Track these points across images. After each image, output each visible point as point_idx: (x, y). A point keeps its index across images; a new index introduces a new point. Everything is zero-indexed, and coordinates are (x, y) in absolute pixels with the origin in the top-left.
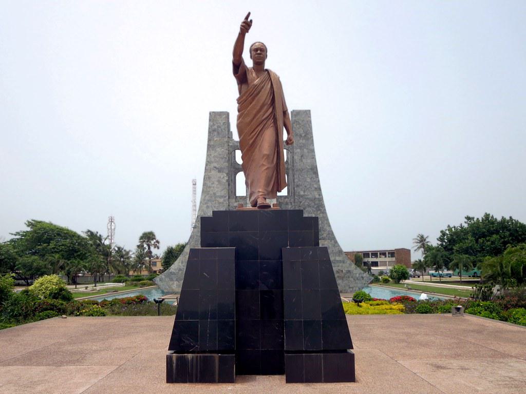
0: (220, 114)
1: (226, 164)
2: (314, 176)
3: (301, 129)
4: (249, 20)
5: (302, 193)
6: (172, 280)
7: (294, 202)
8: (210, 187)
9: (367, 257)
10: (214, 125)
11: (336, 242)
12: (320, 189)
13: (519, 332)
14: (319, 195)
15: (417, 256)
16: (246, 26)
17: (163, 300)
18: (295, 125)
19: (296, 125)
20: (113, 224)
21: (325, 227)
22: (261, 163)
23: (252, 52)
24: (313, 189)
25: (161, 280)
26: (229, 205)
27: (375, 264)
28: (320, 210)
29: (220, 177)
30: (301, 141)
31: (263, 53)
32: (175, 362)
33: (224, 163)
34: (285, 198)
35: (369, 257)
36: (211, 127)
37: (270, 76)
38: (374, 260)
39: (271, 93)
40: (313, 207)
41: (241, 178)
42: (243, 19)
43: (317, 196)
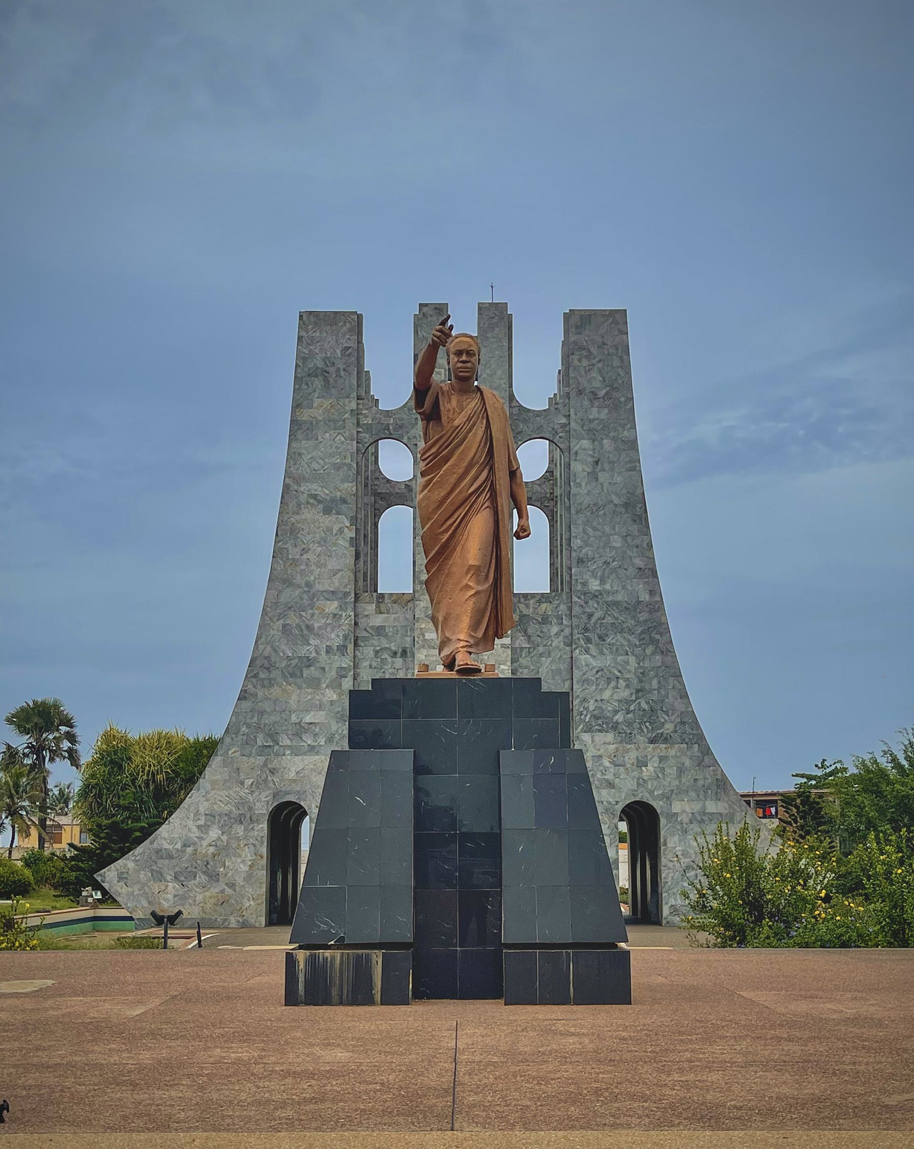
0: (332, 319)
1: (349, 487)
3: (594, 374)
6: (159, 876)
7: (570, 616)
8: (295, 562)
14: (652, 593)
17: (180, 913)
18: (576, 357)
19: (580, 360)
22: (465, 582)
23: (452, 356)
24: (631, 571)
25: (122, 877)
26: (356, 624)
31: (473, 359)
32: (302, 966)
33: (343, 481)
34: (539, 602)
37: (484, 403)
39: (486, 439)
40: (631, 632)
41: (398, 527)
43: (645, 597)
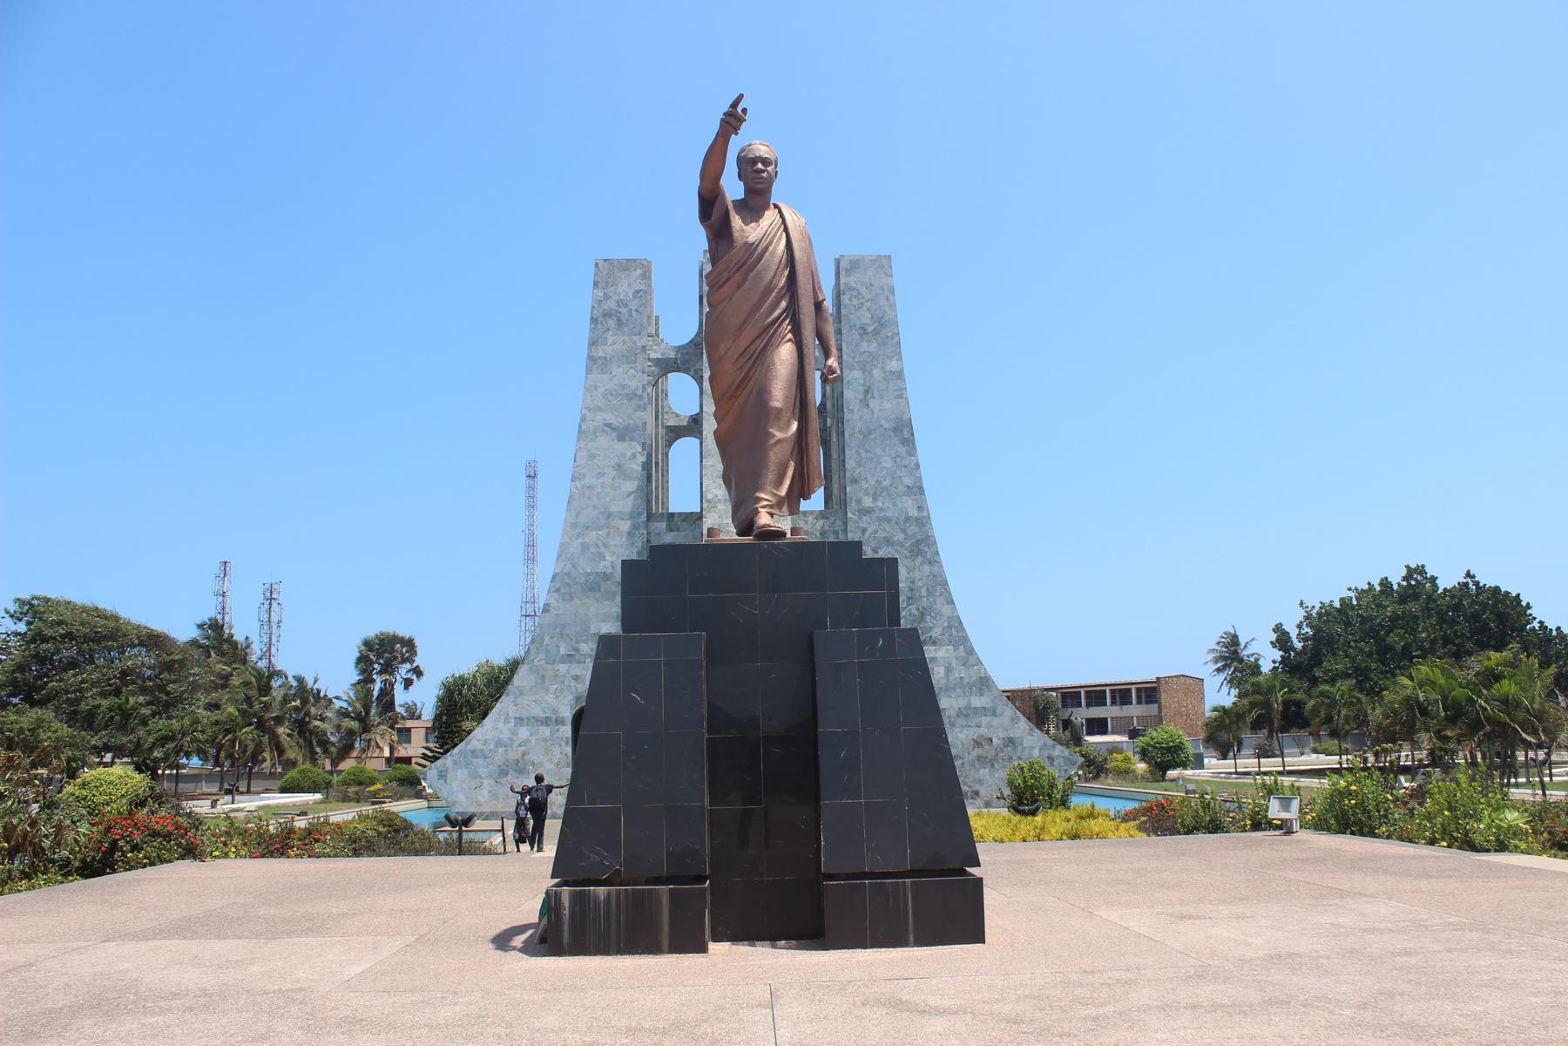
2: (903, 450)
3: (863, 311)
4: (739, 109)
5: (868, 502)
9: (1073, 706)
10: (607, 297)
11: (971, 651)
12: (921, 490)
13: (1414, 857)
14: (920, 508)
15: (1219, 695)
16: (732, 121)
20: (274, 603)
21: (938, 606)
24: (901, 489)
27: (1098, 726)
28: (921, 553)
29: (623, 455)
30: (864, 346)
32: (567, 904)
35: (1079, 705)
36: (600, 302)
38: (1097, 712)
40: (902, 545)
42: (726, 108)
43: (914, 513)
